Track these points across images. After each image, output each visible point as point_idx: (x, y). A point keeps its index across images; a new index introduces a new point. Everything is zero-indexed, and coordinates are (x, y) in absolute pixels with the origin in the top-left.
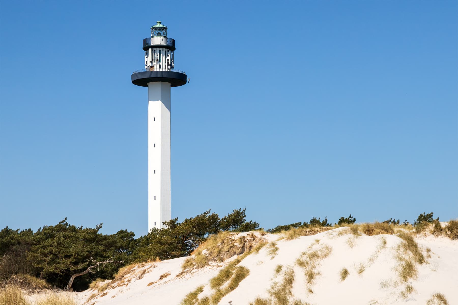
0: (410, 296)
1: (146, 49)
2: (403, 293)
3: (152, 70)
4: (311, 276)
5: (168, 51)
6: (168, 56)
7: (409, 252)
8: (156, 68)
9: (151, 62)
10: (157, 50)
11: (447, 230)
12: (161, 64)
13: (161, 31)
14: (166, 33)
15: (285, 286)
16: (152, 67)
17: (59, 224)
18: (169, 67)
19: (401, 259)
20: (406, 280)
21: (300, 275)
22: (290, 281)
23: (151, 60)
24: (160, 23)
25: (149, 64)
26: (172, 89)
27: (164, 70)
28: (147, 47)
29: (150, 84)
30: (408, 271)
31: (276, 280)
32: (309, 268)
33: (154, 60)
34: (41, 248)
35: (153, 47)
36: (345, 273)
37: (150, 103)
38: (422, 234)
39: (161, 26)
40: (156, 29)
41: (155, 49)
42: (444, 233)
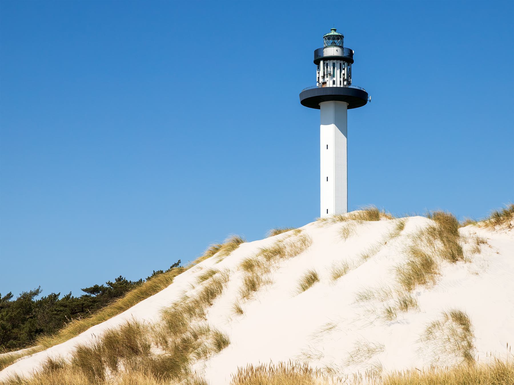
0: (400, 315)
1: (317, 62)
2: (389, 312)
3: (324, 86)
4: (252, 286)
5: (344, 64)
6: (344, 69)
7: (439, 244)
9: (323, 77)
12: (335, 79)
13: (337, 40)
14: (343, 43)
15: (197, 302)
16: (324, 83)
18: (345, 83)
22: (210, 295)
23: (322, 75)
24: (335, 30)
25: (321, 80)
26: (350, 111)
27: (339, 86)
29: (322, 104)
30: (421, 271)
31: (188, 294)
33: (327, 75)
37: (322, 127)
38: (504, 225)
39: (336, 33)
40: (329, 38)
41: (328, 62)
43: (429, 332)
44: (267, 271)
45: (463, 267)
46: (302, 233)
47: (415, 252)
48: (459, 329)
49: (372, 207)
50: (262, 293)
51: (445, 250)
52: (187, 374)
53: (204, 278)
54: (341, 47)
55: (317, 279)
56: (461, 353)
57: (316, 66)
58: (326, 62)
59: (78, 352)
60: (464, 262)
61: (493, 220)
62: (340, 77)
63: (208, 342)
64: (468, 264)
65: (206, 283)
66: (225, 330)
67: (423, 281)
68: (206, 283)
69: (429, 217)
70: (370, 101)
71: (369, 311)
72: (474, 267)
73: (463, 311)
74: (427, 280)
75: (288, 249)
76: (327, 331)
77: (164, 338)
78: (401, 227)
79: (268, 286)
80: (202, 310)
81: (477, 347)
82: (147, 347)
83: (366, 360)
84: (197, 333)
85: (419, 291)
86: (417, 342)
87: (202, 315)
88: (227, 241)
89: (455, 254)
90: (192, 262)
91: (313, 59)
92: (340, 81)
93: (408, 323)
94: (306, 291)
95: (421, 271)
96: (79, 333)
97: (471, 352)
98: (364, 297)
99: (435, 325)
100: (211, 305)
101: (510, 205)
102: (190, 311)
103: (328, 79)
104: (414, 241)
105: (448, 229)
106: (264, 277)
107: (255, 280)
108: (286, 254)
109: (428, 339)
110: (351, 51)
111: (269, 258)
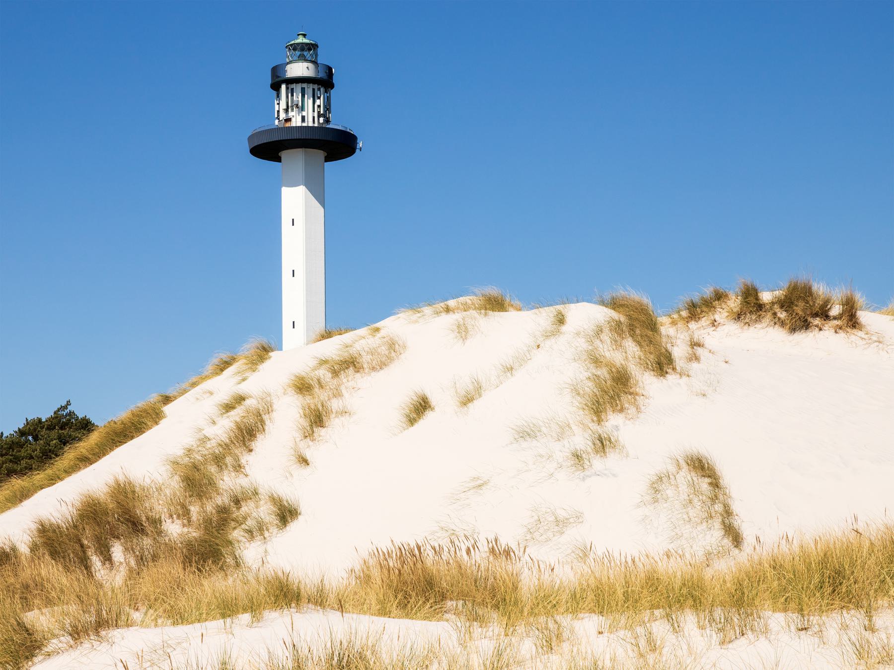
0: (598, 463)
1: (276, 87)
2: (577, 457)
3: (288, 125)
4: (317, 419)
5: (319, 89)
6: (319, 98)
7: (630, 345)
8: (296, 122)
9: (287, 110)
10: (298, 87)
11: (777, 308)
12: (304, 113)
13: (306, 51)
14: (316, 55)
15: (226, 447)
16: (288, 120)
17: (55, 413)
19: (596, 361)
20: (599, 421)
21: (287, 415)
22: (247, 434)
24: (304, 35)
25: (283, 116)
26: (329, 165)
27: (311, 124)
29: (284, 154)
30: (613, 392)
31: (210, 431)
32: (321, 395)
34: (11, 461)
35: (291, 81)
36: (422, 406)
37: (286, 191)
38: (705, 321)
39: (306, 41)
40: (295, 47)
41: (293, 86)
42: (769, 314)
44: (338, 394)
45: (679, 384)
46: (382, 333)
47: (596, 361)
48: (704, 484)
49: (493, 291)
50: (335, 427)
52: (238, 565)
53: (228, 407)
54: (315, 62)
55: (430, 407)
56: (717, 524)
57: (275, 93)
58: (291, 86)
59: (39, 531)
60: (678, 376)
63: (265, 511)
64: (685, 378)
65: (237, 414)
66: (288, 493)
67: (619, 408)
68: (237, 414)
69: (603, 303)
70: (361, 149)
71: (541, 456)
74: (627, 405)
75: (366, 359)
77: (183, 506)
78: (561, 320)
79: (344, 419)
80: (237, 459)
82: (156, 522)
83: (556, 538)
84: (240, 496)
87: (238, 468)
88: (249, 347)
89: (663, 364)
90: (184, 386)
91: (270, 82)
92: (314, 117)
93: (614, 475)
94: (416, 426)
96: (21, 501)
98: (526, 433)
99: (661, 478)
100: (251, 451)
101: (712, 289)
102: (218, 460)
104: (591, 342)
105: (639, 324)
106: (335, 404)
107: (321, 408)
108: (365, 366)
109: (656, 501)
110: (330, 69)
111: (335, 373)
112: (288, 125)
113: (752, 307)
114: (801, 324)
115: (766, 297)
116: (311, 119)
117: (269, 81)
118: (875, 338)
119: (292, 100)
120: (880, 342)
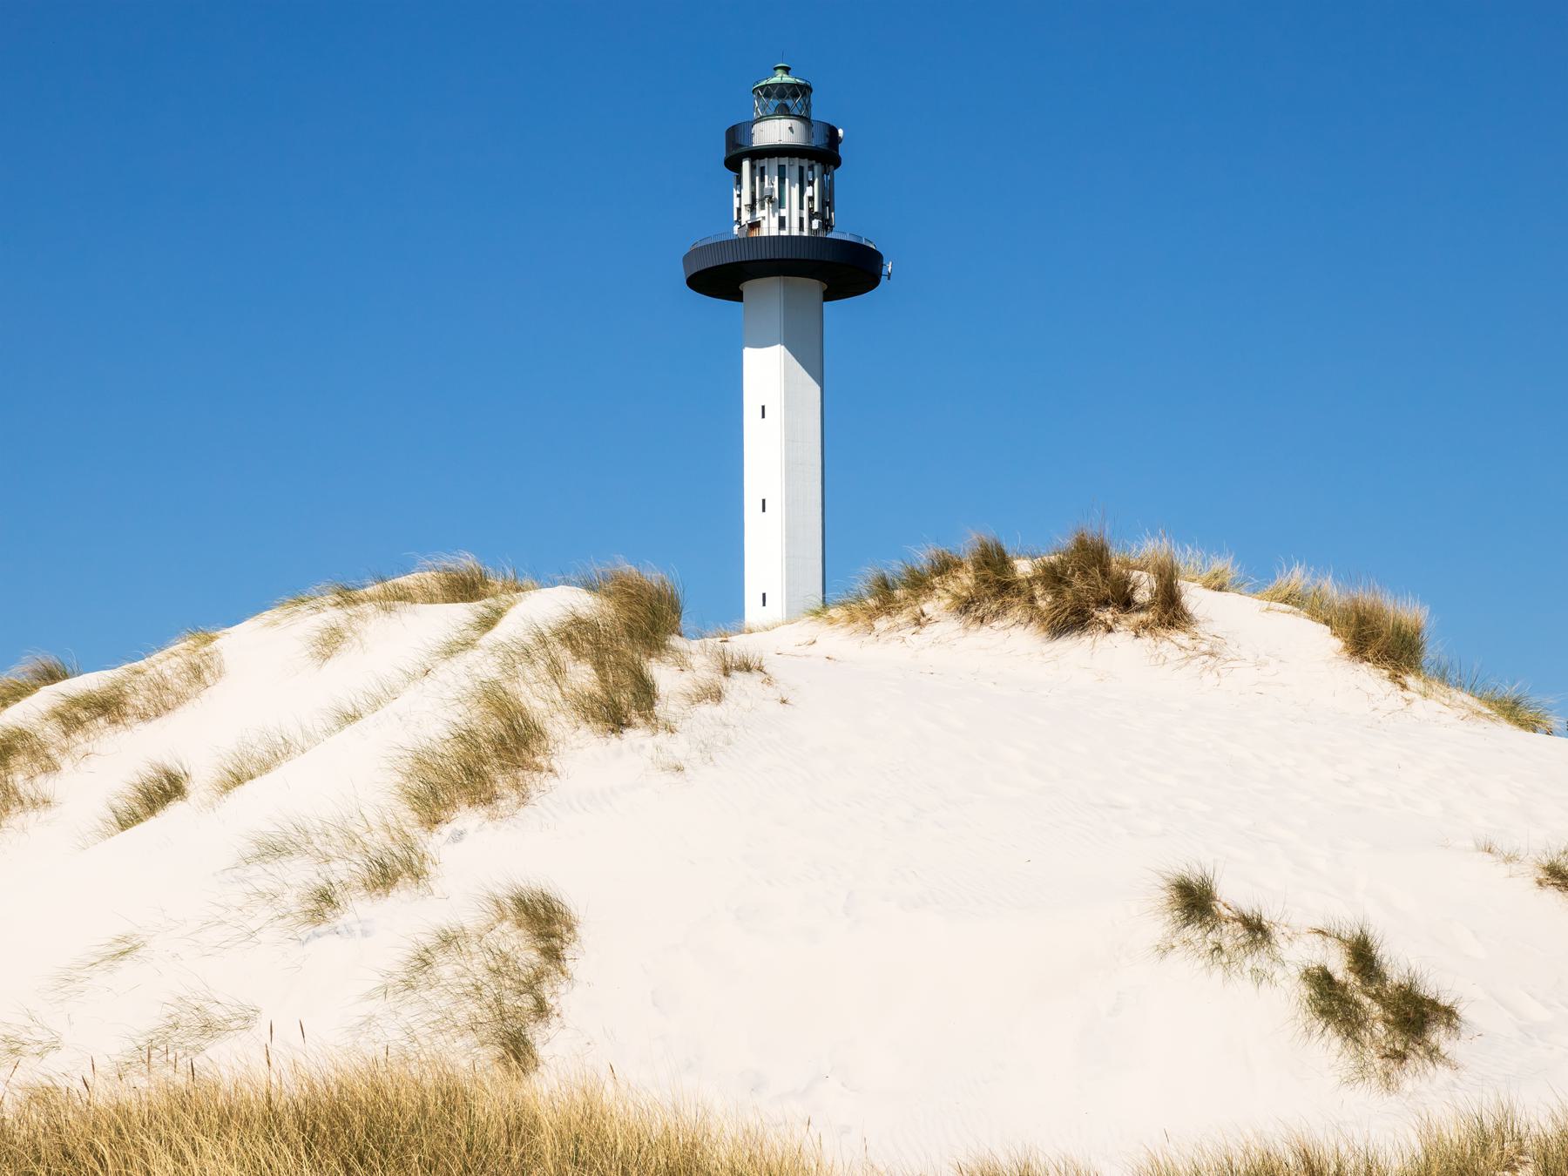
1: (733, 164)
3: (755, 234)
5: (811, 168)
6: (811, 184)
8: (770, 228)
9: (752, 208)
10: (772, 165)
12: (784, 213)
14: (808, 107)
16: (755, 225)
18: (816, 224)
24: (787, 70)
27: (795, 232)
28: (740, 153)
29: (748, 288)
30: (492, 758)
33: (762, 200)
37: (750, 356)
38: (903, 618)
39: (787, 79)
40: (768, 91)
41: (764, 162)
43: (424, 961)
49: (467, 562)
51: (598, 692)
54: (805, 119)
57: (733, 175)
58: (760, 163)
61: (872, 602)
62: (801, 208)
64: (662, 736)
69: (590, 587)
70: (889, 276)
72: (678, 747)
73: (552, 892)
75: (137, 700)
76: (109, 962)
81: (563, 1015)
85: (460, 828)
86: (369, 996)
91: (723, 155)
95: (492, 758)
97: (537, 1034)
103: (764, 213)
104: (508, 666)
110: (833, 131)
112: (755, 234)
113: (994, 586)
114: (1071, 620)
115: (1023, 568)
116: (796, 223)
117: (722, 155)
118: (1205, 647)
119: (762, 187)
120: (1212, 654)
